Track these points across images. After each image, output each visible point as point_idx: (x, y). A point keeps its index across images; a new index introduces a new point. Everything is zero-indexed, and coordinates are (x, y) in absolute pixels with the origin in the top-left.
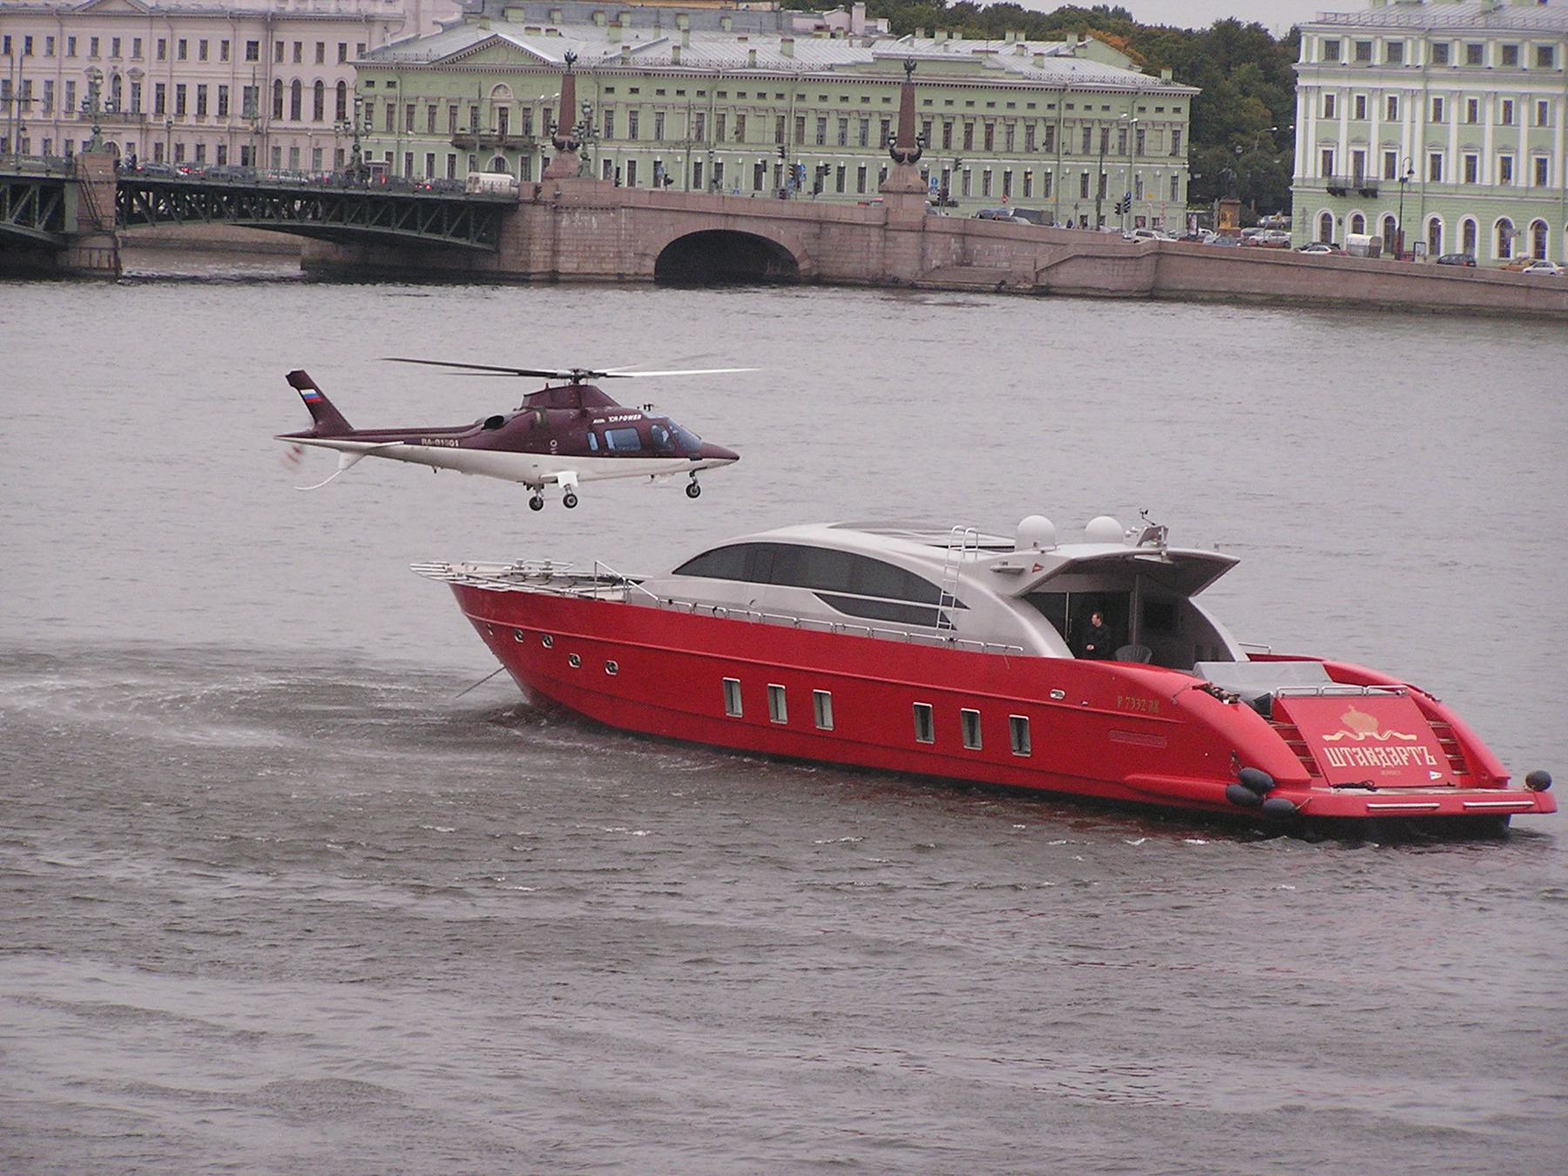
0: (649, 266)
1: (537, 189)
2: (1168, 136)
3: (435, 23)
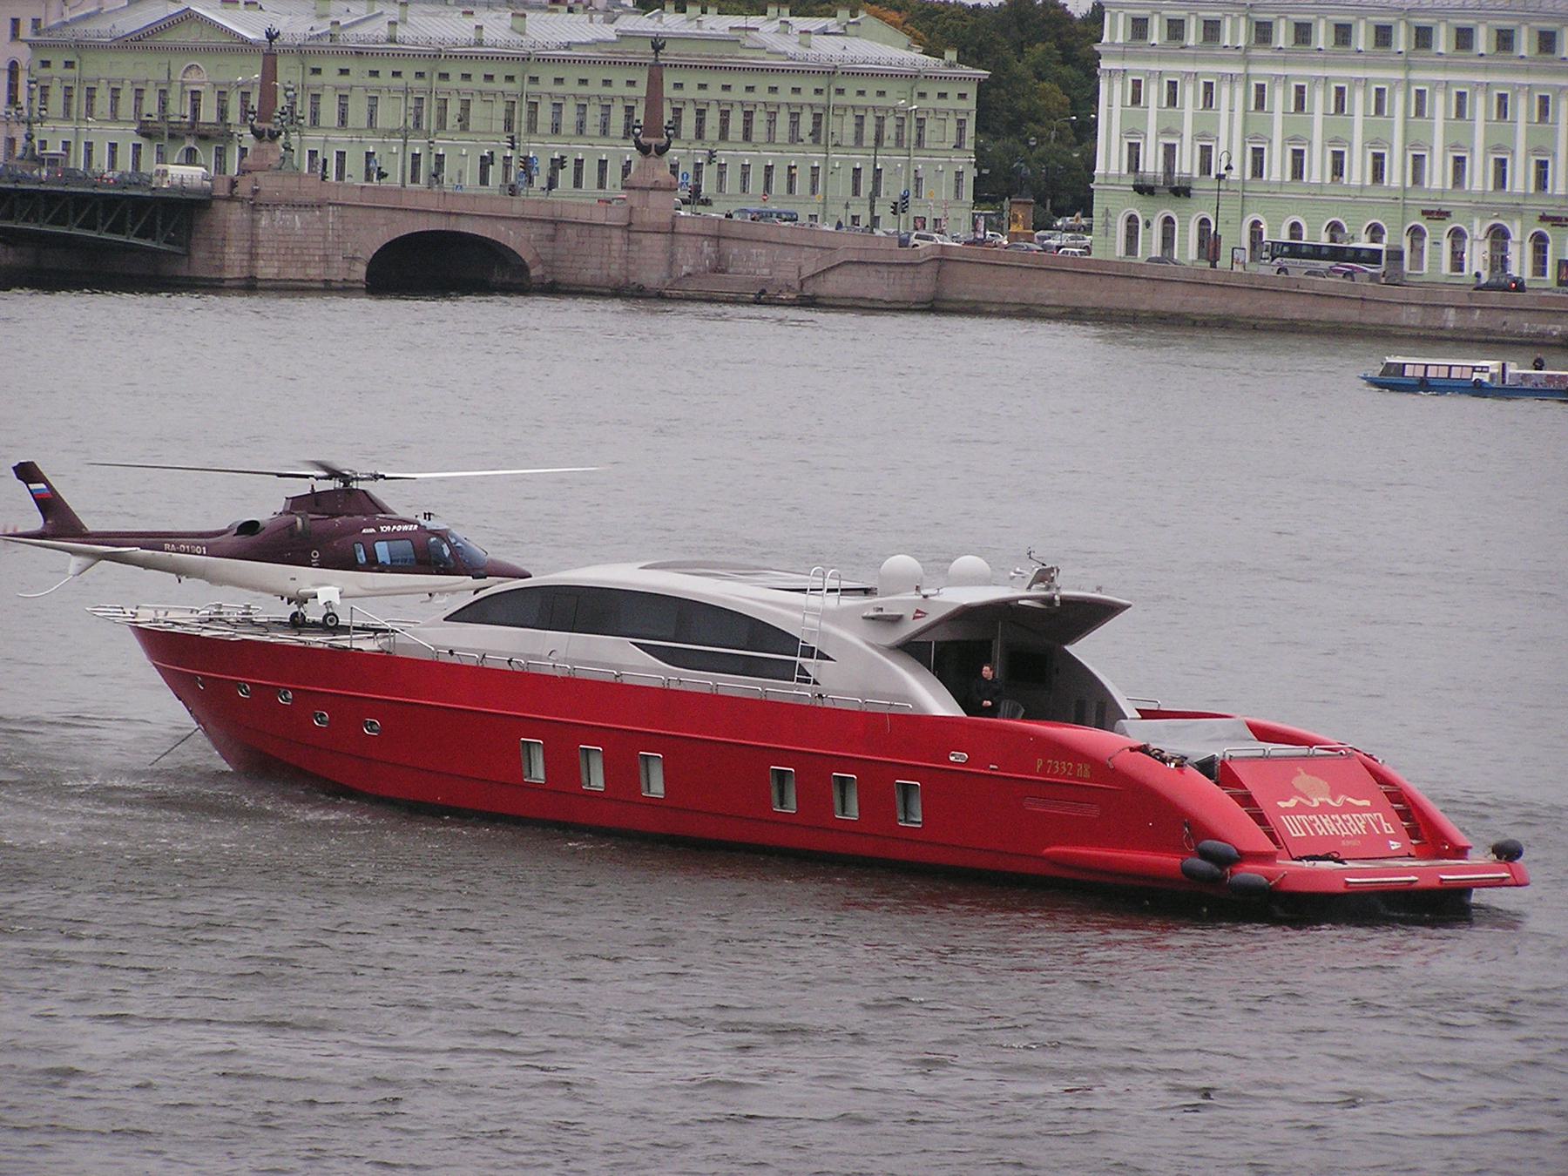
0: (360, 271)
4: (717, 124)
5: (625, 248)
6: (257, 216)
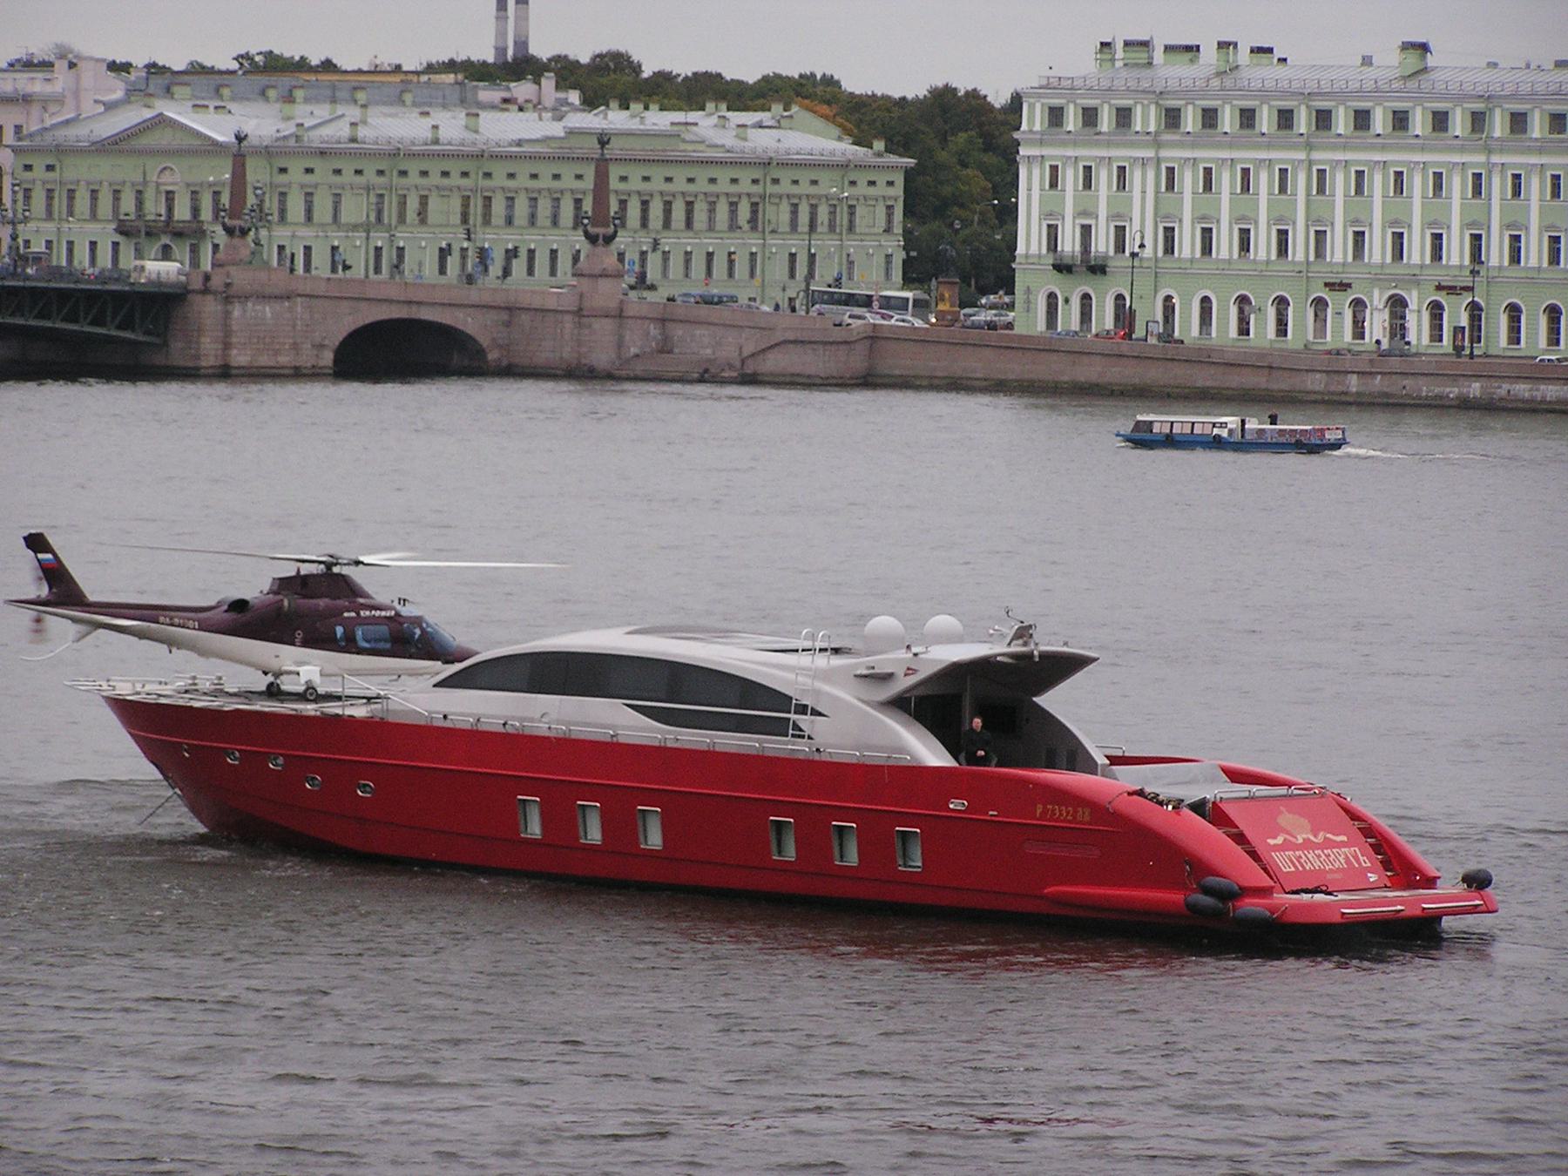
0: (328, 358)
3: (96, 101)
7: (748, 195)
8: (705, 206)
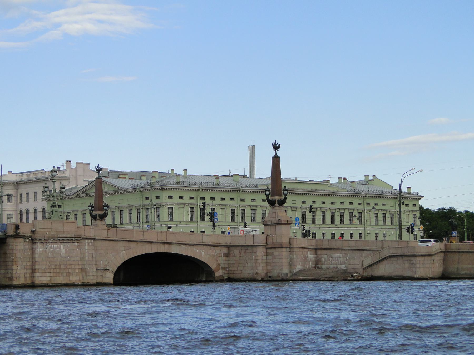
0: (110, 277)
1: (17, 227)
2: (411, 216)
3: (84, 181)
4: (321, 217)
5: (265, 257)
6: (35, 246)
7: (357, 209)
8: (339, 214)
